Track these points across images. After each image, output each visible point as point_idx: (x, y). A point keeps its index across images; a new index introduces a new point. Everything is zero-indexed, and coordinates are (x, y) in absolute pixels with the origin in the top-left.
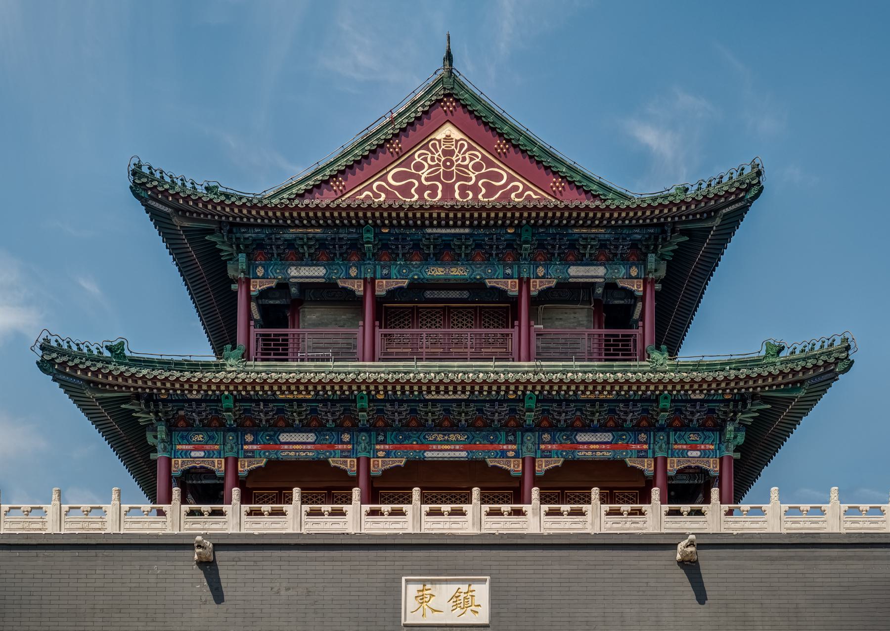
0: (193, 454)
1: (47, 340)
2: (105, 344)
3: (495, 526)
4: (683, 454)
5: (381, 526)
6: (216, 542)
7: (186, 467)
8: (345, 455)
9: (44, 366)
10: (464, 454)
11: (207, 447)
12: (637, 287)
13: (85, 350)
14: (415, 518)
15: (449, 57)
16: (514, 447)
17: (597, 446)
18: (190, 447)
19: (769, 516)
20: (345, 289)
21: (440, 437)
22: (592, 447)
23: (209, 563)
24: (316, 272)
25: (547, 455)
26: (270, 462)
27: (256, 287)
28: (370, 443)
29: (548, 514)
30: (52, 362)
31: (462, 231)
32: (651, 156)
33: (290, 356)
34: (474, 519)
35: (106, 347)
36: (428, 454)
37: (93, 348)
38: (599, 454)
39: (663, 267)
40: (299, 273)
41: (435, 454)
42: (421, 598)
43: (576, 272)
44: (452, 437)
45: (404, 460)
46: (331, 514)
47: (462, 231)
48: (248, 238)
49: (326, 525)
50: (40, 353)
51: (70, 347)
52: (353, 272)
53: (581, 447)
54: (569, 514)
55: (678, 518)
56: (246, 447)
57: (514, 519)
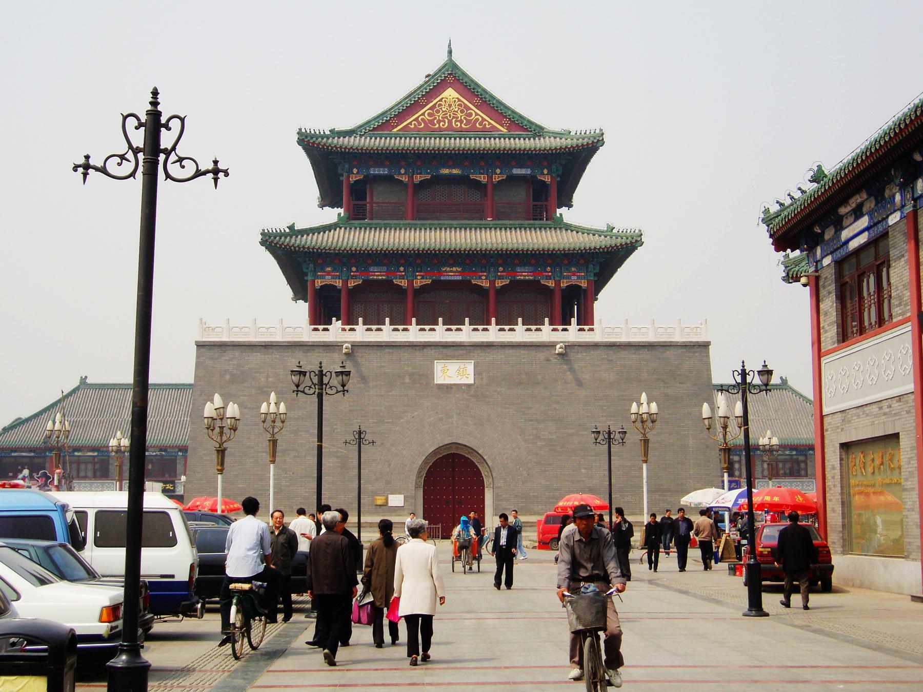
7: (420, 512)
8: (402, 277)
9: (263, 243)
12: (547, 179)
14: (440, 333)
15: (450, 52)
21: (448, 269)
24: (384, 171)
25: (501, 278)
27: (353, 179)
28: (413, 271)
30: (267, 241)
32: (557, 115)
34: (466, 334)
36: (442, 278)
39: (561, 168)
40: (374, 171)
42: (443, 371)
43: (516, 171)
44: (454, 269)
48: (459, 535)
49: (400, 337)
52: (403, 171)
57: (484, 332)
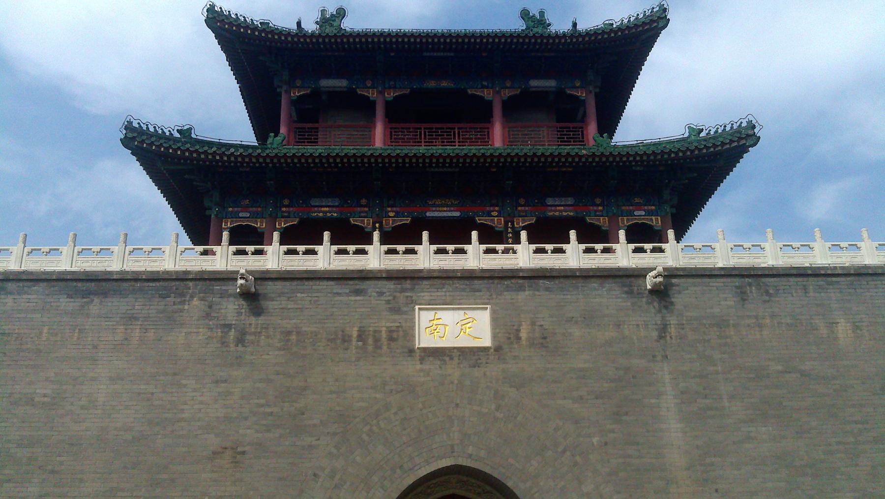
0: (241, 215)
1: (130, 123)
2: (177, 128)
3: (591, 261)
4: (630, 214)
5: (397, 262)
6: (257, 276)
9: (126, 142)
10: (457, 214)
11: (251, 209)
13: (160, 132)
16: (497, 208)
17: (327, 209)
18: (240, 209)
19: (864, 251)
20: (571, 95)
22: (323, 209)
23: (255, 293)
26: (302, 222)
29: (235, 254)
31: (449, 54)
33: (320, 143)
34: (475, 256)
35: (178, 130)
36: (428, 214)
37: (166, 131)
38: (329, 214)
41: (436, 214)
45: (535, 219)
46: (304, 253)
47: (449, 54)
50: (124, 132)
51: (148, 128)
53: (550, 208)
54: (253, 254)
55: (592, 255)
56: (520, 208)
